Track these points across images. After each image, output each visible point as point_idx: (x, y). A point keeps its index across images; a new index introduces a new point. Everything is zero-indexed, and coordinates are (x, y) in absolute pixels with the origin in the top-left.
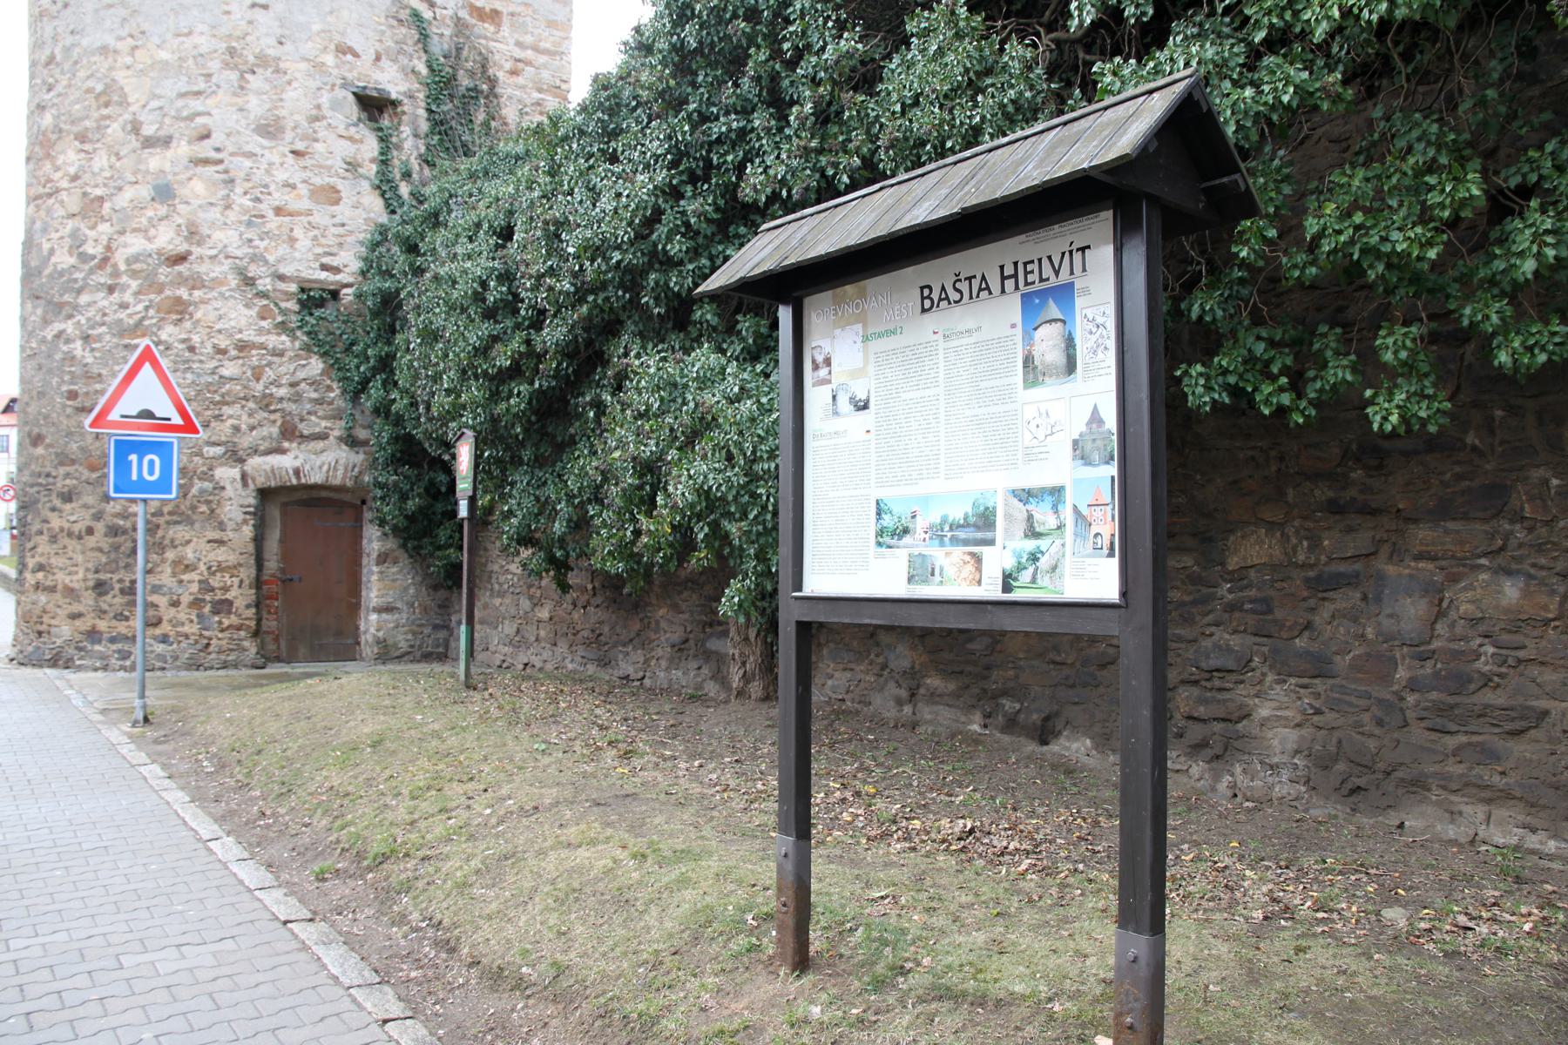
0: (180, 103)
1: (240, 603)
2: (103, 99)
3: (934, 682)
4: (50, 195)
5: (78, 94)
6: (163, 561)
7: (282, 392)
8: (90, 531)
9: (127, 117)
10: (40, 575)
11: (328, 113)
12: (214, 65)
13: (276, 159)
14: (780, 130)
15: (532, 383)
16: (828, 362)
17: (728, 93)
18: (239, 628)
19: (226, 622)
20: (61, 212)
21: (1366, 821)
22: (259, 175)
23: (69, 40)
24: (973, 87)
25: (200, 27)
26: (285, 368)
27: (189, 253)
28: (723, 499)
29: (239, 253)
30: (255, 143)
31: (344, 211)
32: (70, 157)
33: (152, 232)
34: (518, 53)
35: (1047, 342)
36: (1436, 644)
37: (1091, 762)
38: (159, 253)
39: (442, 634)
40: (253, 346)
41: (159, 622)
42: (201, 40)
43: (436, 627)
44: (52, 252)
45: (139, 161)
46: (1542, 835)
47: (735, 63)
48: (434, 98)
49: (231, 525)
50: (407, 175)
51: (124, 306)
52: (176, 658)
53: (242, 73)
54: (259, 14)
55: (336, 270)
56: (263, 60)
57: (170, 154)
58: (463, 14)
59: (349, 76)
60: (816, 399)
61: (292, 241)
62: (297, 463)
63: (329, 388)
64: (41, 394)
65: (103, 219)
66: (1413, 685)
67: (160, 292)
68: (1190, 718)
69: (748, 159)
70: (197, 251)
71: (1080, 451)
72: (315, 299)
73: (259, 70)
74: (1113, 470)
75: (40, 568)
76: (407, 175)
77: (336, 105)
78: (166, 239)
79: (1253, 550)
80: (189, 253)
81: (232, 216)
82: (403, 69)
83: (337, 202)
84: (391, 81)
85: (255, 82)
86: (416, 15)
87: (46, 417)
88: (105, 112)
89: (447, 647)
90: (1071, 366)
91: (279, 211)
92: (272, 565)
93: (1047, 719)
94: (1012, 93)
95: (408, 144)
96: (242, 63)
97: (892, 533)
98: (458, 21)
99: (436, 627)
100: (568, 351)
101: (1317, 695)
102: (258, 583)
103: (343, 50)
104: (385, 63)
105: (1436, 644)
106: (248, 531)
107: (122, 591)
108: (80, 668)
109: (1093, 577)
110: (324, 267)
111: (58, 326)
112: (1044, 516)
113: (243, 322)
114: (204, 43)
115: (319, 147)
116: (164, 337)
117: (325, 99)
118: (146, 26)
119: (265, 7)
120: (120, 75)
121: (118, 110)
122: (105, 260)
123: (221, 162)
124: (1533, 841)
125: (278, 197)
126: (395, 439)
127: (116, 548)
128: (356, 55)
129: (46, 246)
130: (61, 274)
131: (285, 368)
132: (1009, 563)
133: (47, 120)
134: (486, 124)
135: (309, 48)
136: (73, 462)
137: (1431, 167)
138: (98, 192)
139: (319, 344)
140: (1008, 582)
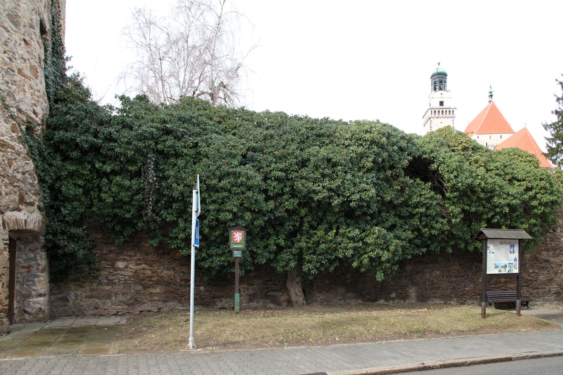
60: (488, 251)
97: (496, 267)
109: (516, 271)
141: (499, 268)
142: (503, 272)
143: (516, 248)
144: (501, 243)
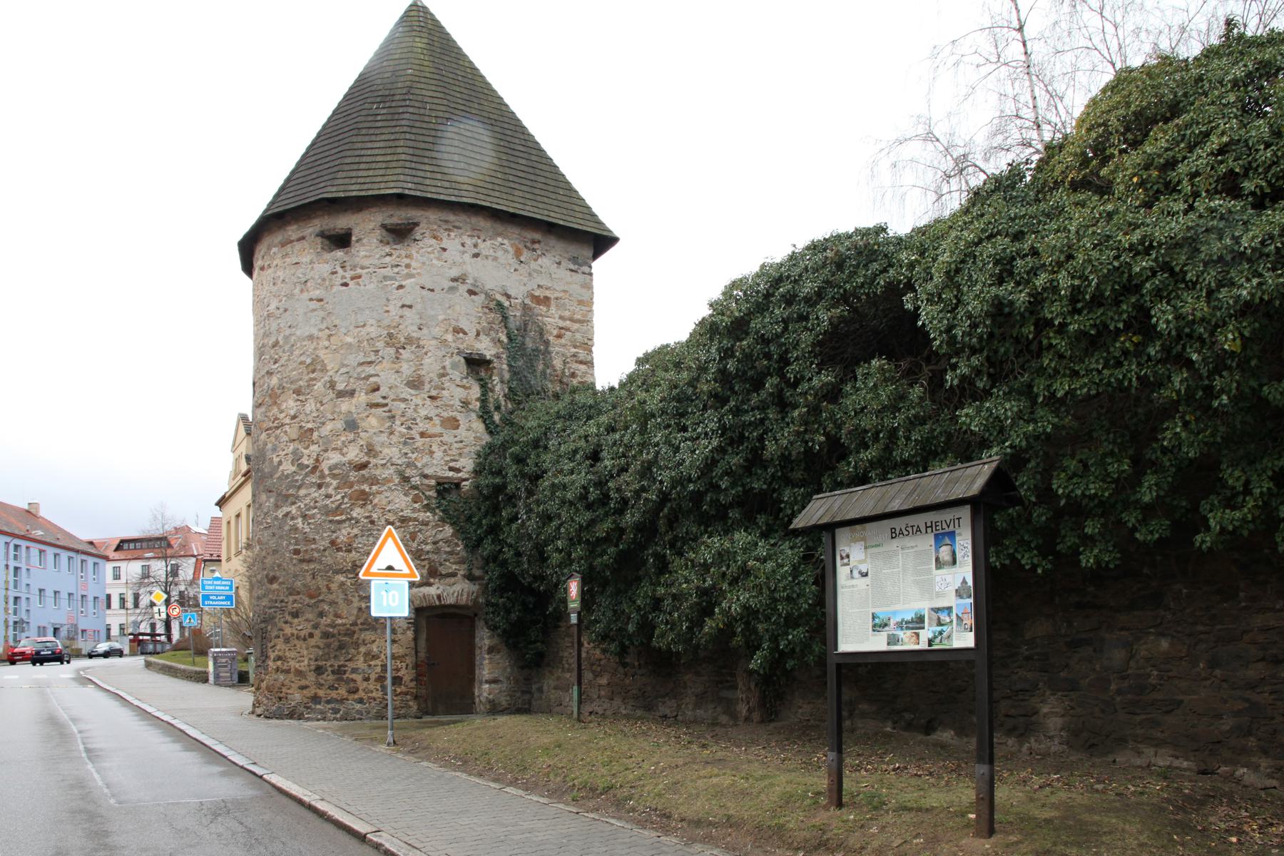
0: (360, 369)
1: (407, 678)
2: (311, 368)
3: (864, 706)
4: (277, 428)
5: (295, 365)
6: (359, 653)
7: (428, 547)
8: (311, 635)
9: (327, 378)
10: (279, 663)
11: (450, 371)
12: (380, 345)
13: (420, 402)
14: (783, 419)
15: (617, 546)
16: (848, 556)
17: (754, 400)
18: (406, 694)
19: (399, 690)
20: (285, 438)
21: (1097, 760)
22: (410, 413)
23: (287, 333)
24: (893, 408)
25: (371, 321)
26: (430, 533)
27: (368, 463)
28: (758, 611)
29: (399, 462)
30: (407, 392)
31: (462, 432)
32: (290, 404)
33: (345, 450)
34: (561, 324)
35: (945, 553)
36: (1130, 672)
37: (954, 742)
38: (350, 463)
39: (527, 697)
40: (410, 519)
41: (357, 690)
42: (372, 329)
43: (524, 692)
44: (280, 463)
45: (335, 406)
46: (1181, 760)
47: (758, 384)
48: (512, 358)
49: (400, 631)
50: (498, 408)
51: (328, 496)
52: (368, 713)
53: (397, 349)
54: (406, 312)
55: (458, 470)
56: (410, 340)
57: (354, 401)
58: (527, 301)
59: (461, 347)
60: (842, 572)
61: (432, 453)
62: (439, 592)
63: (457, 545)
64: (275, 552)
65: (313, 443)
66: (1119, 692)
67: (351, 487)
68: (1007, 716)
69: (765, 432)
70: (373, 461)
71: (959, 593)
72: (445, 488)
73: (408, 347)
74: (971, 600)
75: (279, 658)
76: (498, 408)
77: (454, 366)
78: (354, 454)
79: (1039, 629)
80: (368, 463)
81: (394, 439)
82: (493, 340)
83: (457, 427)
84: (486, 348)
85: (405, 354)
86: (499, 304)
87: (279, 566)
88: (312, 376)
89: (530, 704)
90: (954, 562)
91: (422, 435)
92: (422, 655)
93: (929, 722)
94: (913, 412)
95: (498, 388)
96: (397, 343)
97: (879, 626)
98: (525, 306)
99: (524, 692)
100: (639, 527)
101: (1072, 700)
102: (416, 666)
103: (458, 330)
104: (482, 337)
105: (1130, 672)
106: (410, 634)
107: (333, 672)
108: (308, 719)
109: (965, 640)
110: (451, 469)
111: (286, 509)
112: (945, 618)
113: (403, 505)
114: (373, 331)
115: (445, 393)
116: (355, 515)
117: (448, 363)
118: (337, 322)
119: (410, 307)
120: (321, 353)
121: (321, 374)
122: (315, 468)
123: (386, 405)
124: (1177, 763)
125: (422, 426)
126: (501, 576)
127: (328, 646)
128: (465, 333)
129: (276, 460)
130: (287, 476)
131: (430, 533)
132: (931, 636)
133: (274, 381)
134: (543, 373)
135: (437, 331)
136: (298, 593)
137: (1112, 453)
138: (310, 426)
139: (449, 517)
140: (930, 642)
141: (892, 629)
142: (907, 643)
143: (964, 543)
144: (894, 534)
